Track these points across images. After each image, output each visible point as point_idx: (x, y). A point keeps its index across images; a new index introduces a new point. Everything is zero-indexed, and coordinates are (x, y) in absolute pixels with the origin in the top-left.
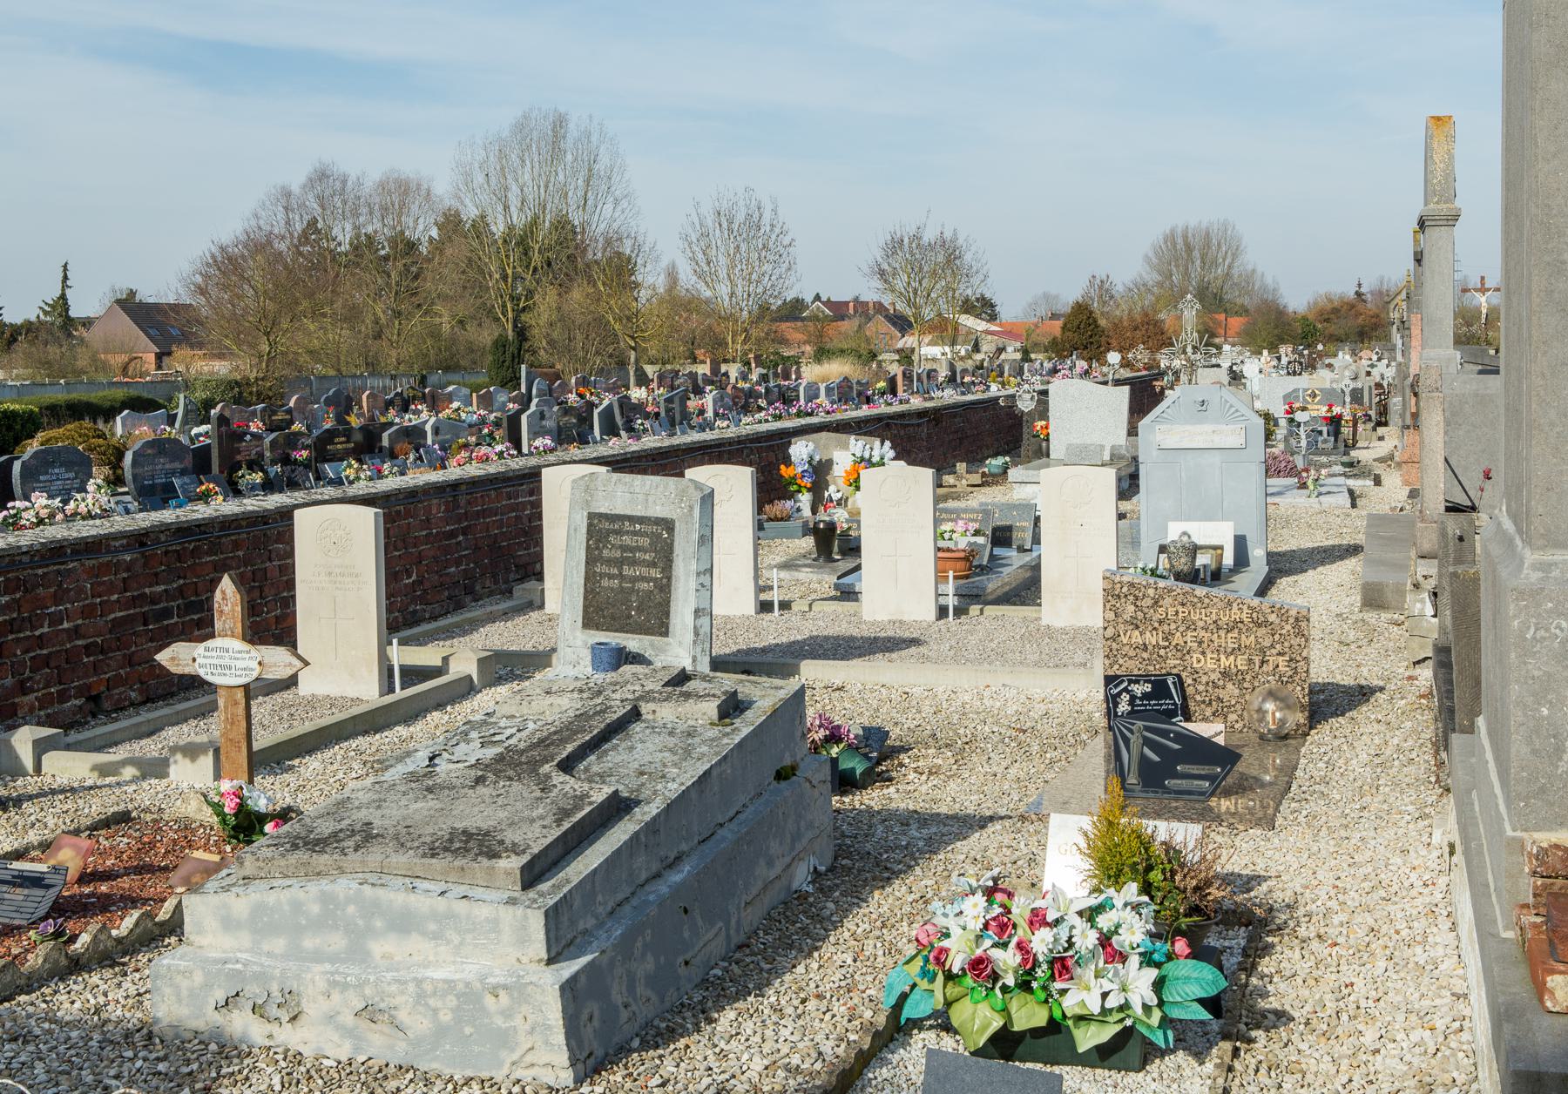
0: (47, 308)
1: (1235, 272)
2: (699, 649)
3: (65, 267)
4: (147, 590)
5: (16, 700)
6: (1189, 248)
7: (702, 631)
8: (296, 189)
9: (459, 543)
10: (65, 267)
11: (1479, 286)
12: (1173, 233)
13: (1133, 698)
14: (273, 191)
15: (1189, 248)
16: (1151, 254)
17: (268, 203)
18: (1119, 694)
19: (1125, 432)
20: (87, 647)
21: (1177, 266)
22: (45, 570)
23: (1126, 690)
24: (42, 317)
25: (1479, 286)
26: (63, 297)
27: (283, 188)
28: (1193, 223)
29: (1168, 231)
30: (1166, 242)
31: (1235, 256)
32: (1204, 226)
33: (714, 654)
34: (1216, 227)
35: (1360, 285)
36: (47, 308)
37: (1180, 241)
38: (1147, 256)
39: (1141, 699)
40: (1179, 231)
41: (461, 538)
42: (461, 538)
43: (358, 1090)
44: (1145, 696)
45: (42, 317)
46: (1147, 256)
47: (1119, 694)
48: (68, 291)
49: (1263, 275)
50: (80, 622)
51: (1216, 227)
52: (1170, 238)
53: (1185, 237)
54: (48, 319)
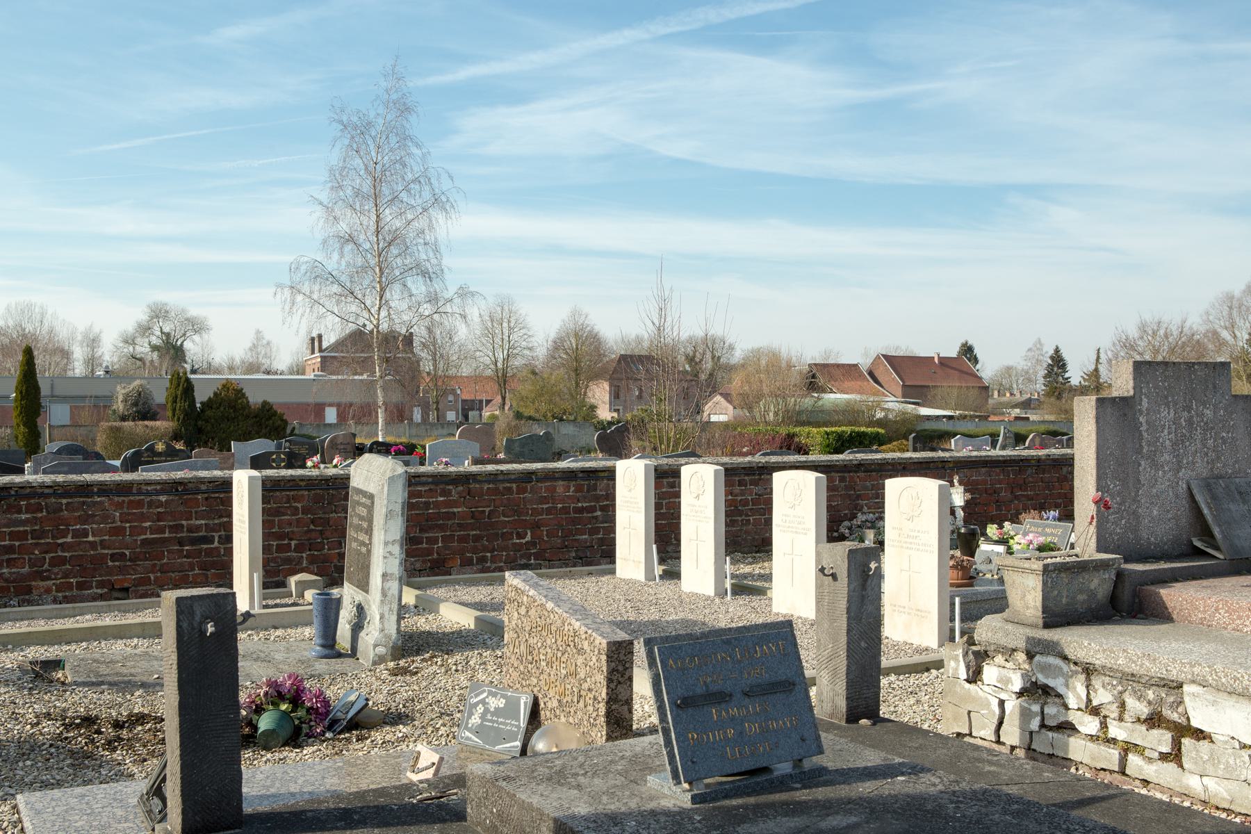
0: (1085, 376)
2: (386, 608)
4: (184, 522)
5: (33, 583)
7: (390, 594)
8: (1237, 293)
9: (596, 518)
10: (1099, 350)
13: (486, 711)
14: (1221, 296)
17: (1217, 304)
18: (477, 704)
19: (1075, 458)
20: (112, 555)
22: (70, 500)
23: (483, 702)
24: (1083, 382)
26: (1096, 370)
27: (1227, 294)
36: (1085, 376)
39: (493, 714)
41: (599, 513)
42: (599, 513)
44: (498, 712)
45: (1083, 382)
47: (477, 704)
48: (1099, 366)
50: (107, 538)
54: (1086, 384)
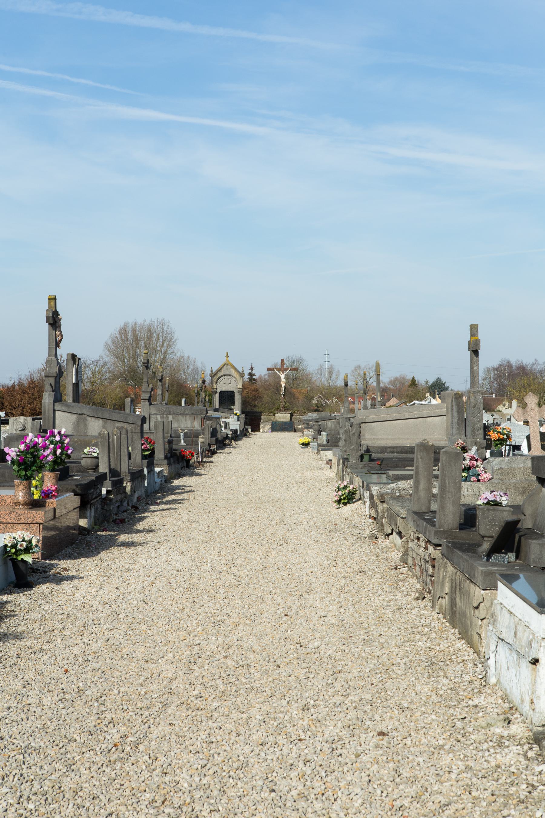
1: (170, 357)
3: (474, 330)
6: (137, 339)
8: (263, 375)
10: (474, 330)
11: (279, 366)
12: (125, 326)
15: (137, 339)
16: (110, 343)
21: (128, 352)
25: (279, 366)
28: (139, 321)
29: (122, 326)
31: (169, 346)
32: (148, 322)
33: (112, 467)
34: (156, 324)
35: (252, 369)
37: (130, 333)
38: (107, 344)
40: (130, 327)
43: (484, 816)
46: (107, 344)
49: (195, 361)
51: (156, 324)
52: (123, 331)
53: (134, 330)
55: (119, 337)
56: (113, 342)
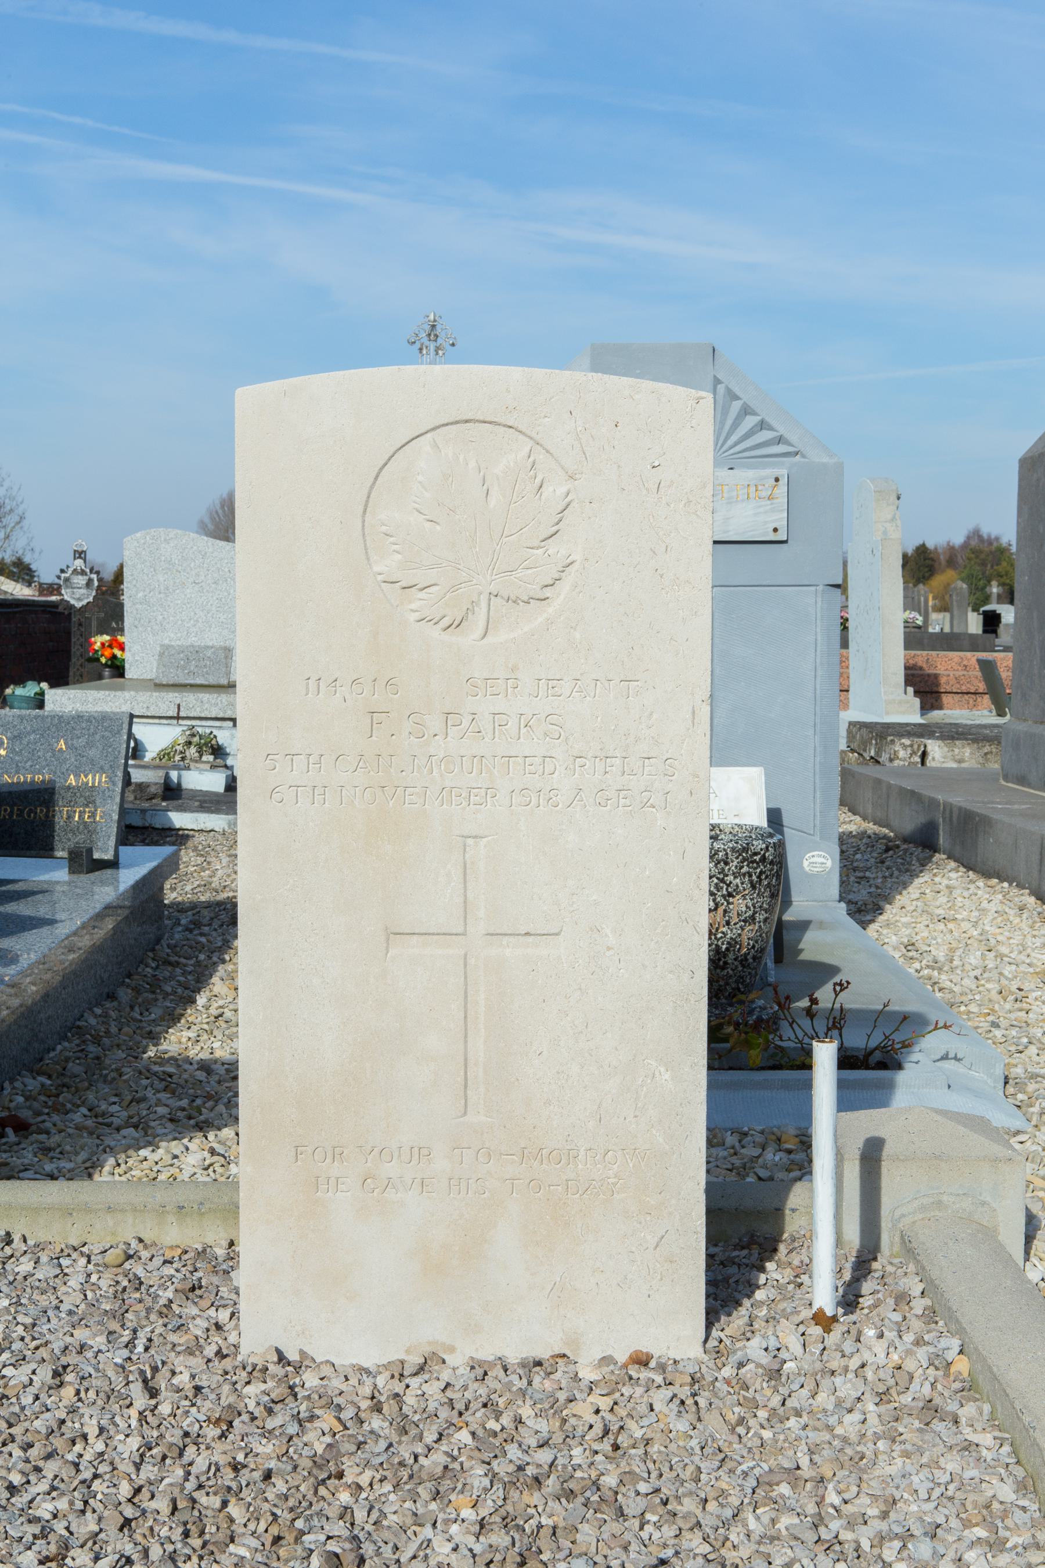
16: (207, 520)
30: (222, 507)
55: (220, 512)
56: (212, 519)
